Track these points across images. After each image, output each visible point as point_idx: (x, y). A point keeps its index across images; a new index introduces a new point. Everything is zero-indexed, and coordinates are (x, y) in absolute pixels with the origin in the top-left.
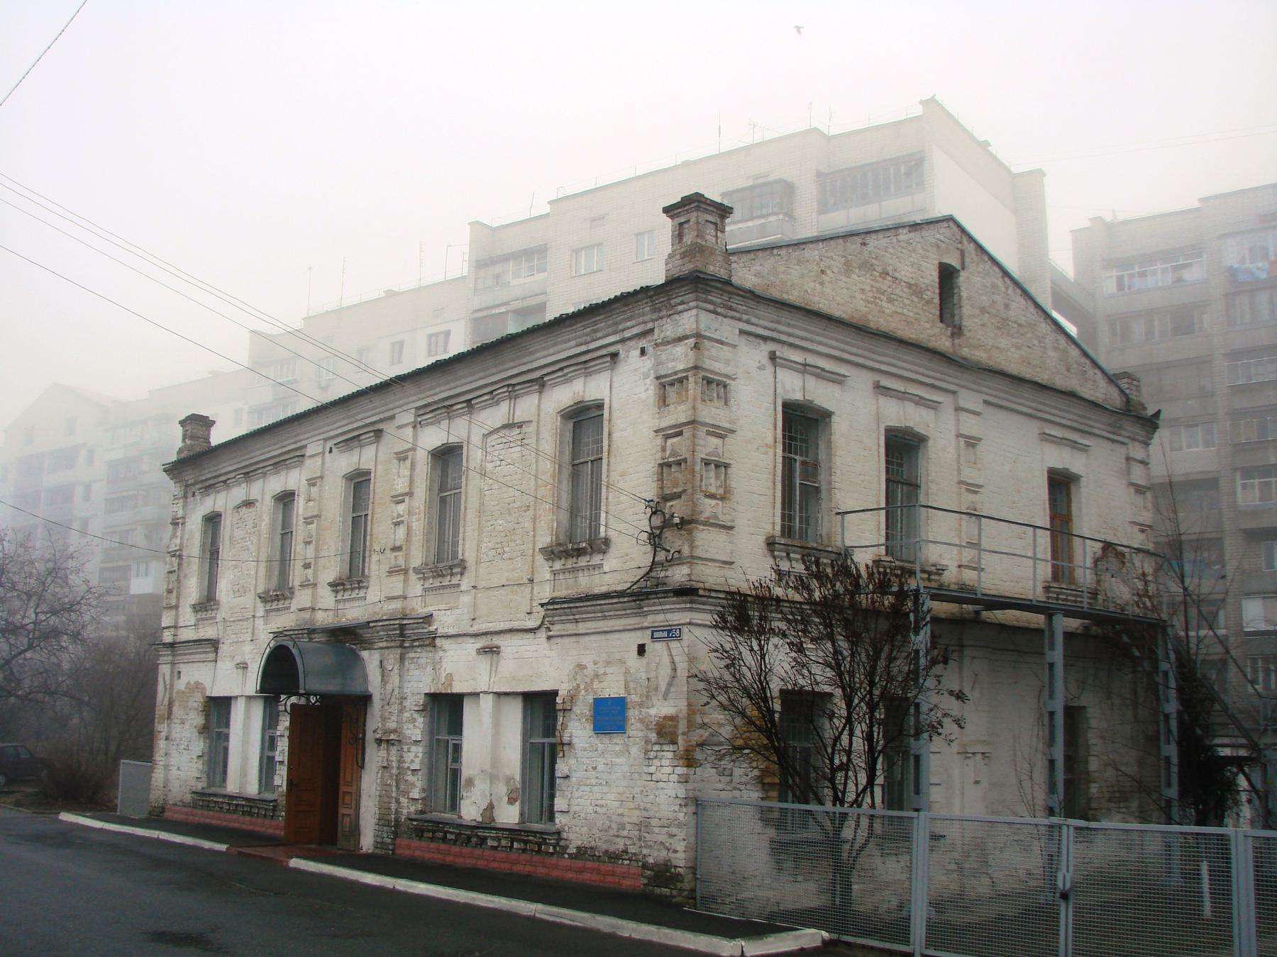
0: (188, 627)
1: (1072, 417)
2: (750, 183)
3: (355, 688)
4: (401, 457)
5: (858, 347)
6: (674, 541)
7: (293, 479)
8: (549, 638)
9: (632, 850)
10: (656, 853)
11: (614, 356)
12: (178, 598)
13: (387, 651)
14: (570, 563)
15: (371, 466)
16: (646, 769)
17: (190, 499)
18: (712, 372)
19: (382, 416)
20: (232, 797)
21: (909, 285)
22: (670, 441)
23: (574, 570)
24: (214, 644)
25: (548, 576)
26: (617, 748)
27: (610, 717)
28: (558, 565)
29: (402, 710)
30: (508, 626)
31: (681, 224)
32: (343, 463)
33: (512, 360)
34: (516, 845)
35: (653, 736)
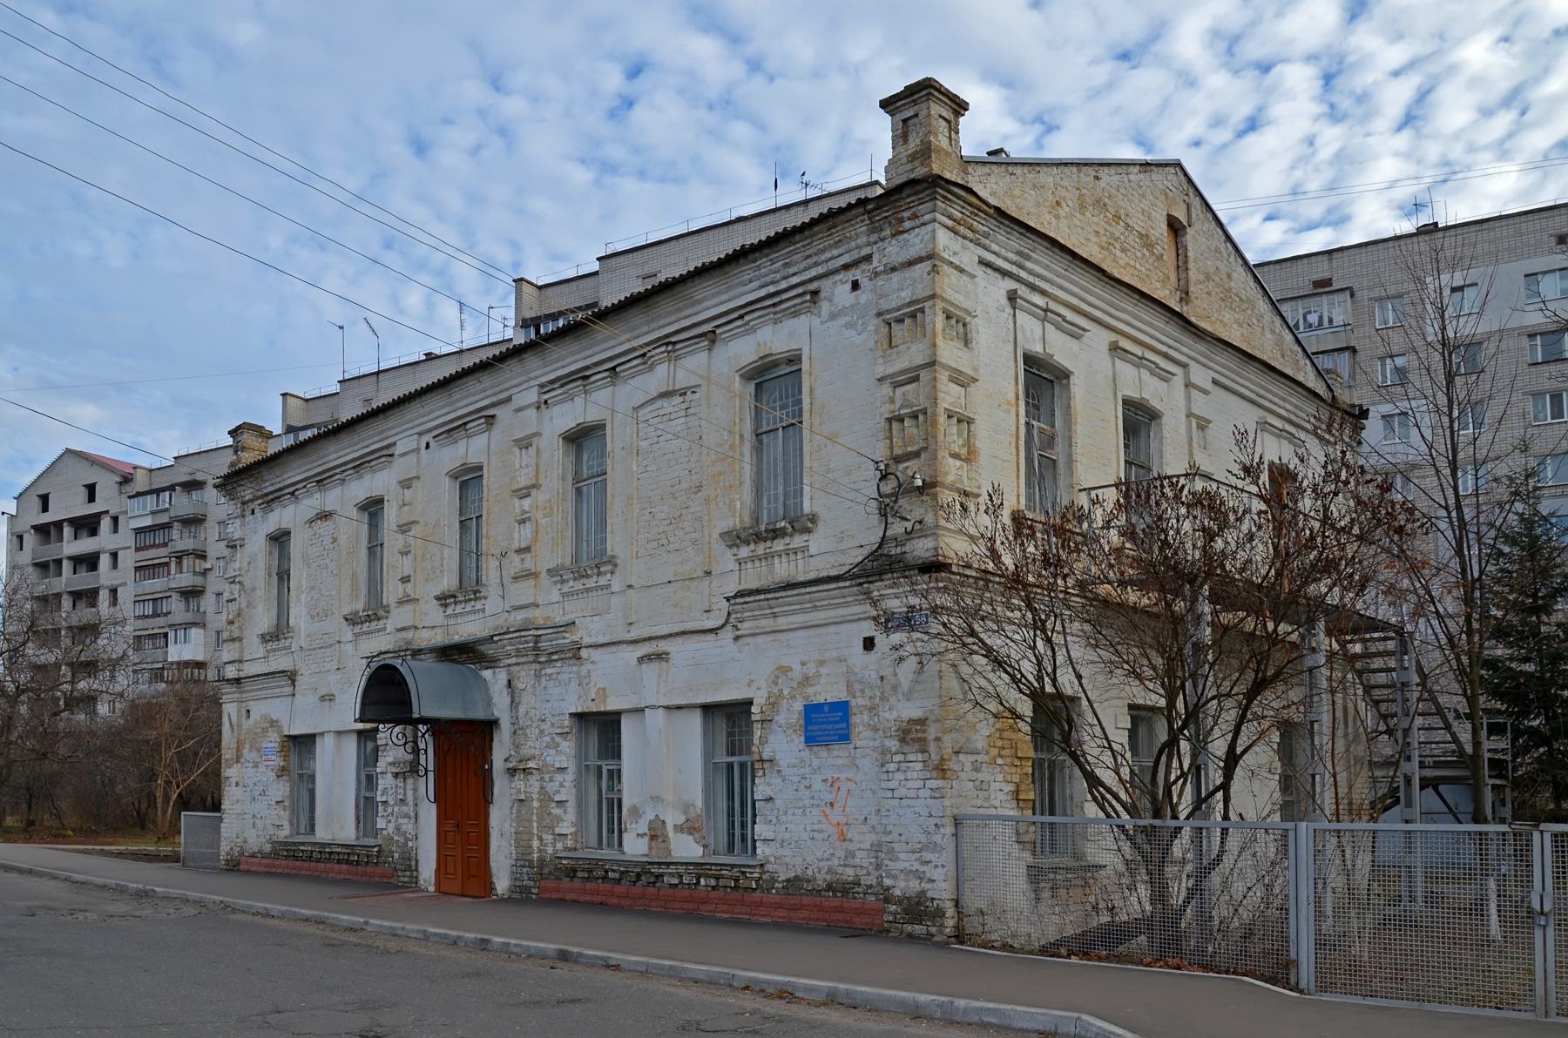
0: (257, 658)
1: (1288, 407)
3: (479, 714)
4: (524, 443)
5: (1099, 298)
6: (914, 509)
9: (865, 881)
10: (902, 884)
11: (815, 293)
13: (516, 668)
14: (761, 549)
15: (483, 459)
16: (884, 785)
17: (249, 518)
18: (952, 304)
19: (494, 399)
20: (323, 845)
21: (1141, 236)
22: (899, 391)
23: (767, 557)
24: (291, 676)
25: (733, 565)
26: (840, 761)
27: (826, 724)
28: (744, 552)
31: (905, 121)
32: (452, 455)
33: (670, 314)
34: (703, 881)
35: (893, 744)
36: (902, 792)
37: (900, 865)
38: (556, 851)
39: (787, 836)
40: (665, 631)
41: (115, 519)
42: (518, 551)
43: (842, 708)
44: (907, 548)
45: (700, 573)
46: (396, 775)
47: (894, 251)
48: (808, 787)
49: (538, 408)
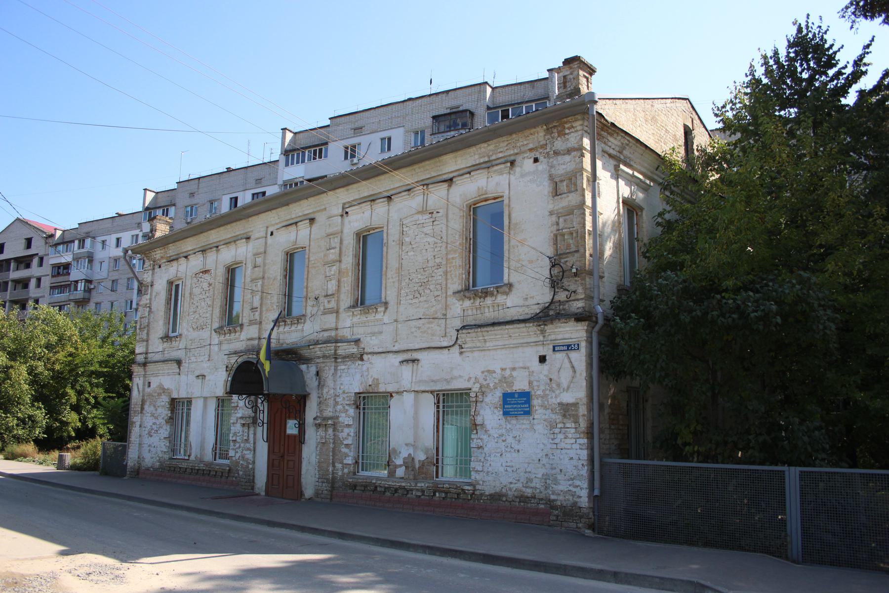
2: (448, 111)
7: (241, 252)
8: (461, 353)
12: (148, 334)
17: (157, 270)
26: (524, 426)
29: (336, 403)
30: (424, 346)
34: (437, 494)
35: (558, 418)
36: (563, 445)
37: (561, 488)
38: (344, 474)
39: (490, 469)
40: (417, 347)
41: (41, 259)
42: (327, 296)
43: (526, 396)
44: (566, 306)
45: (439, 315)
46: (243, 425)
47: (559, 144)
48: (504, 441)
49: (342, 216)
